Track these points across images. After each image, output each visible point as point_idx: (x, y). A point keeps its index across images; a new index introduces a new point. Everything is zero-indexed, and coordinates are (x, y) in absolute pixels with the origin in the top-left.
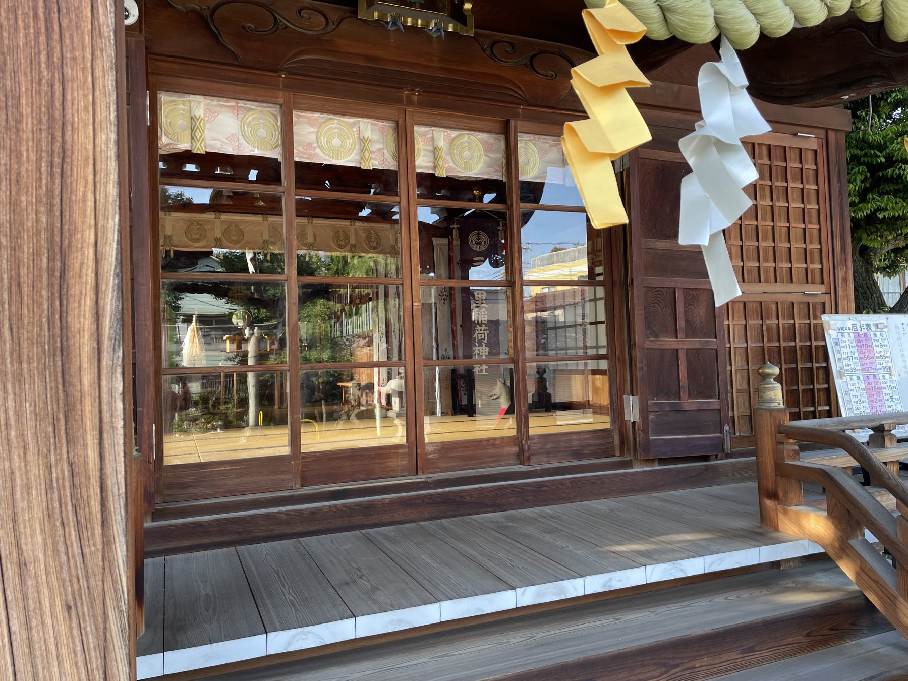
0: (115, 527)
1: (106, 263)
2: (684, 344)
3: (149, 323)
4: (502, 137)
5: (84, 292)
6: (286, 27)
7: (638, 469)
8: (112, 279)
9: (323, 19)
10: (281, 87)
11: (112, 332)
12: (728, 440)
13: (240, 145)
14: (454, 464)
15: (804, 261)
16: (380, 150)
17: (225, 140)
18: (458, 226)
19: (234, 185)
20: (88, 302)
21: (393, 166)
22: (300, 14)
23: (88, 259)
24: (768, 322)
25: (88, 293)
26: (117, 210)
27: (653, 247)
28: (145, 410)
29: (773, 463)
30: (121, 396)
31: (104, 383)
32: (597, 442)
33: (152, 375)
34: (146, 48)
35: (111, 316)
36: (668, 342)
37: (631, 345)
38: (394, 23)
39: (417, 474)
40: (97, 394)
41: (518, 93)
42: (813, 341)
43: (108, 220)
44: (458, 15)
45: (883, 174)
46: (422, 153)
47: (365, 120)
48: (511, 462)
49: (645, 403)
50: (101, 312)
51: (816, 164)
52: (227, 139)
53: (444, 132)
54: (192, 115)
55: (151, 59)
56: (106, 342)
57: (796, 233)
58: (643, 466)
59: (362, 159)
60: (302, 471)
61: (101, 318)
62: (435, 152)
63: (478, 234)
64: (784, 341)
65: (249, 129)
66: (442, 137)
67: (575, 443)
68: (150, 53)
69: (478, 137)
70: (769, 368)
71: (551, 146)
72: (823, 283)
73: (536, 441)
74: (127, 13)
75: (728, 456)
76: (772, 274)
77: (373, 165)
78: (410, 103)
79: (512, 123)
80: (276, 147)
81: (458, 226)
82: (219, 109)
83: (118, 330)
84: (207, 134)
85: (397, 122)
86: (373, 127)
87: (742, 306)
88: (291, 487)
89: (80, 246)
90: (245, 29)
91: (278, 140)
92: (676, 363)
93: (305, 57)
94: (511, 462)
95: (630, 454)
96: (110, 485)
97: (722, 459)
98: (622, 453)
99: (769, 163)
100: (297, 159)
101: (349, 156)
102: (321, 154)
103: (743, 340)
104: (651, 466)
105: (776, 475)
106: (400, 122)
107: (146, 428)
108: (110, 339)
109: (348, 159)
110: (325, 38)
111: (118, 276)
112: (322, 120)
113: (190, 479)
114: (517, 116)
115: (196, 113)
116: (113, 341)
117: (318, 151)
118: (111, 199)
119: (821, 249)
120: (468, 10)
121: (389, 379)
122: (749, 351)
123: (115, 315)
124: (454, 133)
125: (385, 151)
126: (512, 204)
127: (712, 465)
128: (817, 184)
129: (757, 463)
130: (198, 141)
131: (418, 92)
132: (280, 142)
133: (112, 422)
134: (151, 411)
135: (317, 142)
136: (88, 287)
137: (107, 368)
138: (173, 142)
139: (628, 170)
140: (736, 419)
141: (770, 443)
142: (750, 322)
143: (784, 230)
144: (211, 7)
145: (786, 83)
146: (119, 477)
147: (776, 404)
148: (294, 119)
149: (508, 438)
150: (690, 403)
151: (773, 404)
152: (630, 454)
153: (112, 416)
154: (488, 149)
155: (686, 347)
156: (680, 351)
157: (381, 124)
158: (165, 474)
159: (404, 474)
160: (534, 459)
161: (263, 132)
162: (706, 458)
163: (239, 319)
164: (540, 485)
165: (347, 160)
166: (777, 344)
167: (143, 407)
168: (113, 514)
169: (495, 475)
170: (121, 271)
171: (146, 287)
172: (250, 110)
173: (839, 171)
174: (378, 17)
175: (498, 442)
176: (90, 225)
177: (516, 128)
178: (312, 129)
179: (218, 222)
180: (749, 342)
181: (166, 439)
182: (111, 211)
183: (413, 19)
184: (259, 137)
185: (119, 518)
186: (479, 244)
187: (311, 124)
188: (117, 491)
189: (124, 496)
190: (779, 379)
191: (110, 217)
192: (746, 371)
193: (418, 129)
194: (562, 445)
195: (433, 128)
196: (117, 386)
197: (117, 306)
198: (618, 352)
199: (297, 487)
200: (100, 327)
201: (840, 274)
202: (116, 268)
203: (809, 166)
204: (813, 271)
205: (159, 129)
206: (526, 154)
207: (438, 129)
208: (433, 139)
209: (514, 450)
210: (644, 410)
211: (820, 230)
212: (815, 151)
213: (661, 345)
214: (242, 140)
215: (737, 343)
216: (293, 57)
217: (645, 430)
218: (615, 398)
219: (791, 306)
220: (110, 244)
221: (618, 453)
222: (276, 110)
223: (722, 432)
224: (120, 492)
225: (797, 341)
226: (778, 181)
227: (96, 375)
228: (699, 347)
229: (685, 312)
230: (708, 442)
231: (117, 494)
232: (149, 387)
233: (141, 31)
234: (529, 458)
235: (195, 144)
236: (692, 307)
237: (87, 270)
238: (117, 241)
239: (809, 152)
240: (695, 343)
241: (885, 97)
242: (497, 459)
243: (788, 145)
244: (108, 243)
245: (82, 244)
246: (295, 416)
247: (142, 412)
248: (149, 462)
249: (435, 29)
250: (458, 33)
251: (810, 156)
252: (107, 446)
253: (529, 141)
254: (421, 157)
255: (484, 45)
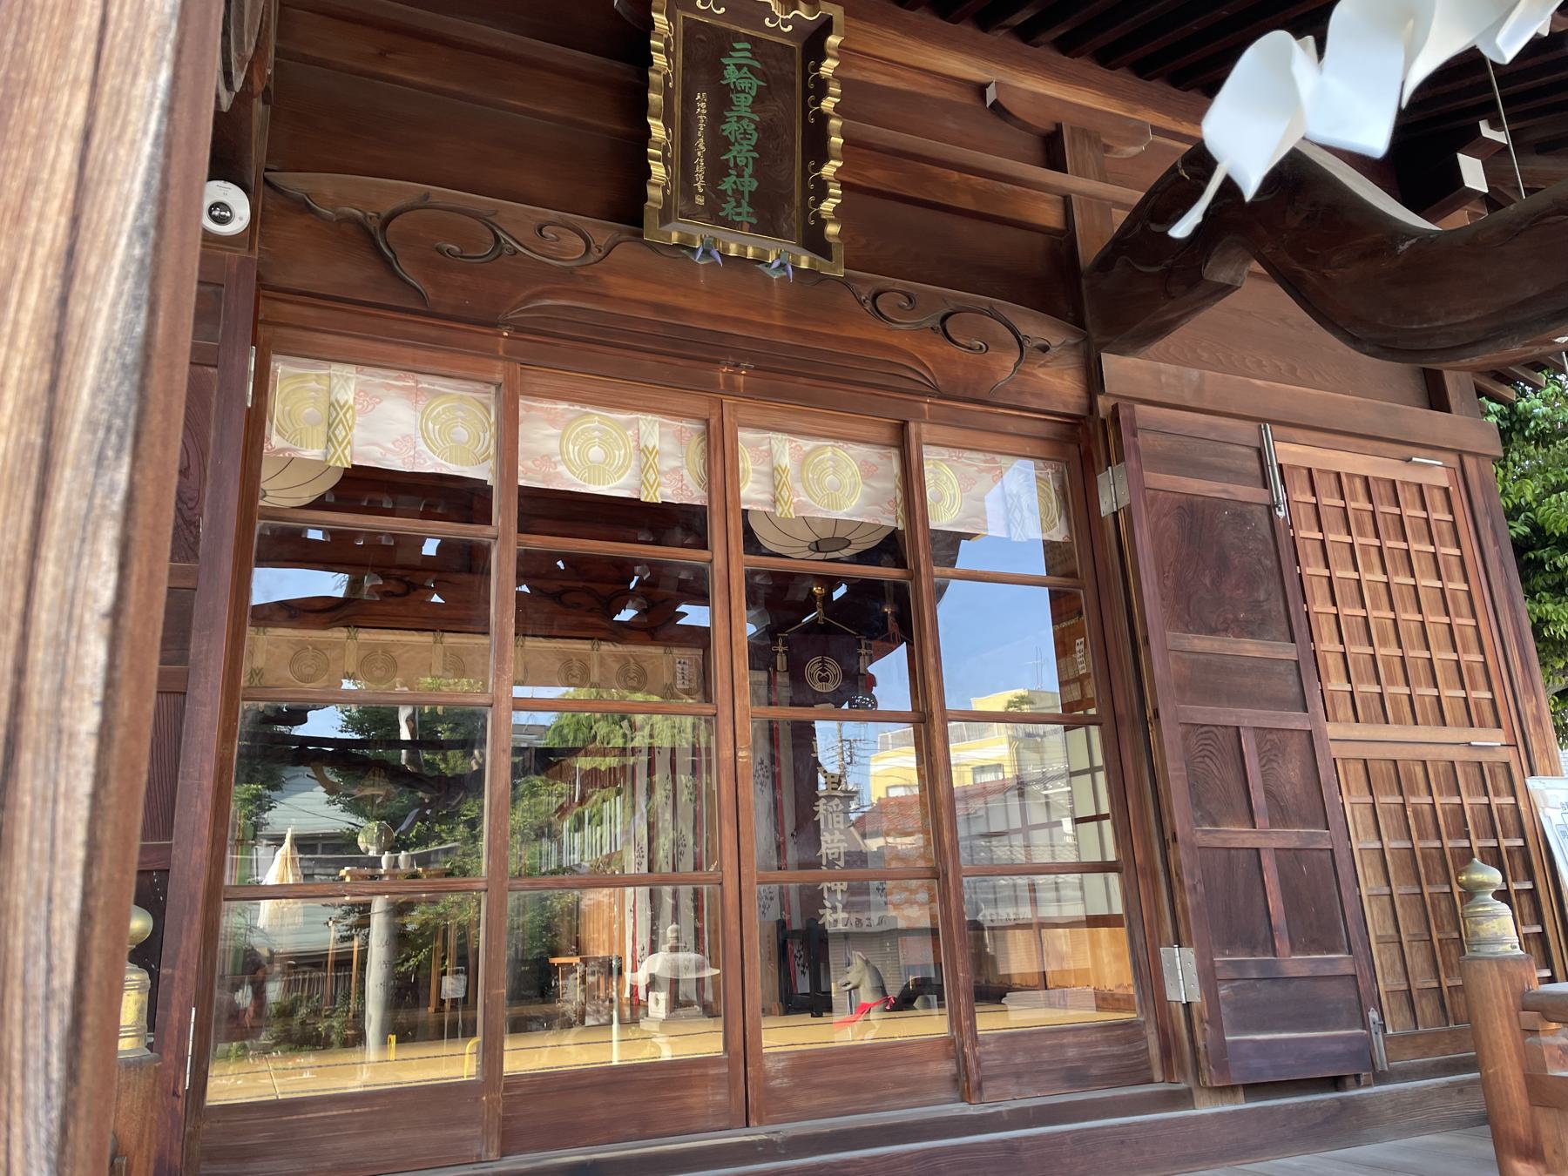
0: (17, 1130)
1: (113, 194)
2: (1270, 838)
3: (208, 783)
4: (894, 454)
5: (23, 264)
6: (516, 252)
7: (1206, 1108)
8: (123, 241)
9: (581, 242)
10: (501, 353)
11: (101, 404)
12: (1379, 1041)
13: (417, 455)
14: (823, 1101)
15: (1459, 685)
16: (675, 470)
17: (390, 446)
18: (786, 648)
19: (403, 523)
20: (32, 299)
21: (698, 497)
22: (540, 231)
23: (53, 171)
24: (1413, 800)
25: (38, 273)
26: (168, 49)
27: (1189, 648)
28: (178, 974)
29: (1521, 1080)
30: (106, 623)
31: (49, 572)
32: (1117, 1050)
33: (200, 896)
34: (259, 278)
35: (105, 352)
36: (1238, 835)
37: (1167, 841)
38: (706, 253)
39: (748, 1125)
40: (18, 605)
41: (926, 378)
42: (1501, 838)
43: (135, 75)
44: (815, 241)
45: (1535, 557)
46: (751, 476)
47: (650, 417)
48: (943, 1096)
49: (1208, 962)
50: (72, 337)
51: (1451, 512)
52: (393, 443)
53: (790, 441)
54: (333, 399)
55: (265, 297)
56: (75, 435)
57: (1437, 634)
58: (1216, 1105)
59: (643, 483)
60: (505, 1119)
61: (68, 357)
62: (775, 475)
63: (823, 661)
64: (1449, 837)
65: (437, 427)
66: (786, 449)
67: (1071, 1053)
68: (264, 287)
69: (851, 452)
70: (1481, 871)
71: (981, 471)
72: (1499, 727)
73: (991, 1048)
74: (228, 214)
75: (1381, 1078)
76: (1407, 709)
77: (662, 496)
78: (732, 390)
79: (912, 427)
80: (484, 460)
81: (786, 648)
82: (382, 392)
83: (122, 400)
84: (358, 434)
85: (707, 422)
86: (663, 429)
87: (1360, 767)
88: (479, 1156)
89: (33, 130)
90: (443, 254)
91: (488, 448)
92: (1259, 877)
93: (548, 302)
94: (943, 1096)
95: (1185, 1075)
96: (20, 954)
97: (1368, 1085)
98: (1168, 1075)
99: (1370, 507)
100: (522, 482)
101: (619, 478)
102: (568, 475)
103: (1373, 836)
104: (1230, 1103)
105: (1532, 1105)
106: (713, 421)
107: (175, 1015)
108: (91, 425)
109: (618, 483)
110: (585, 273)
111: (144, 234)
112: (571, 416)
113: (259, 1139)
114: (920, 417)
115: (339, 397)
116: (101, 434)
117: (562, 468)
118: (153, 21)
119: (1485, 663)
120: (834, 236)
121: (653, 949)
122: (1388, 857)
123: (118, 351)
124: (807, 445)
125: (685, 472)
126: (918, 567)
127: (1352, 1099)
128: (1459, 546)
129: (1484, 1083)
130: (340, 444)
131: (747, 368)
132: (492, 450)
133: (57, 712)
134: (191, 977)
135: (562, 453)
136: (41, 252)
137: (67, 521)
138: (293, 447)
139: (1128, 511)
140: (1383, 999)
141: (1508, 1033)
142: (1382, 799)
143: (1415, 627)
144: (384, 214)
145: (1440, 323)
146: (56, 923)
147: (1508, 947)
148: (521, 413)
149: (933, 1042)
150: (1295, 963)
151: (1500, 948)
152: (1185, 1075)
153: (60, 690)
154: (868, 472)
155: (1274, 845)
156: (1263, 854)
157: (677, 424)
158: (205, 1127)
159: (721, 1125)
160: (990, 1089)
161: (462, 433)
162: (1336, 1083)
163: (371, 844)
164: (1010, 1147)
165: (615, 486)
166: (1437, 844)
167: (174, 968)
168: (16, 1074)
169: (915, 1124)
170: (160, 223)
171: (208, 708)
172: (437, 394)
173: (1493, 527)
174: (678, 240)
175: (913, 1051)
176: (76, 79)
177: (919, 436)
178: (554, 431)
179: (352, 644)
180: (1385, 839)
181: (213, 1071)
182: (147, 54)
183: (740, 246)
184: (453, 441)
185: (36, 1088)
186: (824, 680)
187: (552, 423)
188: (41, 980)
189: (67, 1000)
190: (1503, 896)
191: (143, 67)
192: (1387, 899)
193: (745, 436)
194: (1045, 1056)
195: (771, 434)
196: (94, 584)
197: (128, 326)
198: (1139, 857)
199: (493, 1155)
200: (62, 385)
201: (1528, 709)
202: (141, 209)
203: (1440, 515)
204: (1477, 702)
205: (268, 423)
206: (936, 484)
207: (780, 436)
208: (770, 452)
209: (948, 1068)
210: (1208, 977)
211: (1477, 627)
212: (1446, 490)
213: (1224, 840)
214: (422, 447)
215: (1363, 841)
216: (525, 302)
217: (1215, 1022)
218: (1142, 955)
219: (1450, 769)
220: (133, 142)
221: (1158, 1075)
222: (489, 395)
223: (1365, 1024)
224: (56, 983)
225: (1473, 837)
226: (1389, 539)
227: (25, 535)
228: (1298, 844)
229: (1263, 775)
230: (1339, 1048)
231: (41, 992)
232: (191, 922)
233: (251, 248)
234: (979, 1087)
235: (332, 450)
236: (1275, 765)
237: (46, 202)
238: (157, 136)
239: (1436, 491)
240: (1291, 836)
241: (1517, 426)
242: (914, 1090)
243: (1398, 477)
244: (128, 137)
245: (41, 128)
246: (494, 992)
247: (172, 977)
248: (175, 1094)
249: (776, 264)
250: (818, 272)
251: (1438, 497)
252: (27, 799)
253: (941, 460)
254: (749, 484)
255: (860, 294)
